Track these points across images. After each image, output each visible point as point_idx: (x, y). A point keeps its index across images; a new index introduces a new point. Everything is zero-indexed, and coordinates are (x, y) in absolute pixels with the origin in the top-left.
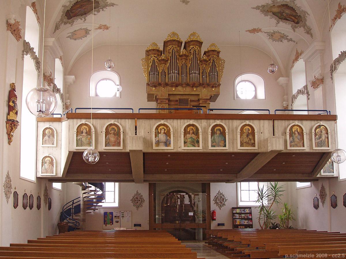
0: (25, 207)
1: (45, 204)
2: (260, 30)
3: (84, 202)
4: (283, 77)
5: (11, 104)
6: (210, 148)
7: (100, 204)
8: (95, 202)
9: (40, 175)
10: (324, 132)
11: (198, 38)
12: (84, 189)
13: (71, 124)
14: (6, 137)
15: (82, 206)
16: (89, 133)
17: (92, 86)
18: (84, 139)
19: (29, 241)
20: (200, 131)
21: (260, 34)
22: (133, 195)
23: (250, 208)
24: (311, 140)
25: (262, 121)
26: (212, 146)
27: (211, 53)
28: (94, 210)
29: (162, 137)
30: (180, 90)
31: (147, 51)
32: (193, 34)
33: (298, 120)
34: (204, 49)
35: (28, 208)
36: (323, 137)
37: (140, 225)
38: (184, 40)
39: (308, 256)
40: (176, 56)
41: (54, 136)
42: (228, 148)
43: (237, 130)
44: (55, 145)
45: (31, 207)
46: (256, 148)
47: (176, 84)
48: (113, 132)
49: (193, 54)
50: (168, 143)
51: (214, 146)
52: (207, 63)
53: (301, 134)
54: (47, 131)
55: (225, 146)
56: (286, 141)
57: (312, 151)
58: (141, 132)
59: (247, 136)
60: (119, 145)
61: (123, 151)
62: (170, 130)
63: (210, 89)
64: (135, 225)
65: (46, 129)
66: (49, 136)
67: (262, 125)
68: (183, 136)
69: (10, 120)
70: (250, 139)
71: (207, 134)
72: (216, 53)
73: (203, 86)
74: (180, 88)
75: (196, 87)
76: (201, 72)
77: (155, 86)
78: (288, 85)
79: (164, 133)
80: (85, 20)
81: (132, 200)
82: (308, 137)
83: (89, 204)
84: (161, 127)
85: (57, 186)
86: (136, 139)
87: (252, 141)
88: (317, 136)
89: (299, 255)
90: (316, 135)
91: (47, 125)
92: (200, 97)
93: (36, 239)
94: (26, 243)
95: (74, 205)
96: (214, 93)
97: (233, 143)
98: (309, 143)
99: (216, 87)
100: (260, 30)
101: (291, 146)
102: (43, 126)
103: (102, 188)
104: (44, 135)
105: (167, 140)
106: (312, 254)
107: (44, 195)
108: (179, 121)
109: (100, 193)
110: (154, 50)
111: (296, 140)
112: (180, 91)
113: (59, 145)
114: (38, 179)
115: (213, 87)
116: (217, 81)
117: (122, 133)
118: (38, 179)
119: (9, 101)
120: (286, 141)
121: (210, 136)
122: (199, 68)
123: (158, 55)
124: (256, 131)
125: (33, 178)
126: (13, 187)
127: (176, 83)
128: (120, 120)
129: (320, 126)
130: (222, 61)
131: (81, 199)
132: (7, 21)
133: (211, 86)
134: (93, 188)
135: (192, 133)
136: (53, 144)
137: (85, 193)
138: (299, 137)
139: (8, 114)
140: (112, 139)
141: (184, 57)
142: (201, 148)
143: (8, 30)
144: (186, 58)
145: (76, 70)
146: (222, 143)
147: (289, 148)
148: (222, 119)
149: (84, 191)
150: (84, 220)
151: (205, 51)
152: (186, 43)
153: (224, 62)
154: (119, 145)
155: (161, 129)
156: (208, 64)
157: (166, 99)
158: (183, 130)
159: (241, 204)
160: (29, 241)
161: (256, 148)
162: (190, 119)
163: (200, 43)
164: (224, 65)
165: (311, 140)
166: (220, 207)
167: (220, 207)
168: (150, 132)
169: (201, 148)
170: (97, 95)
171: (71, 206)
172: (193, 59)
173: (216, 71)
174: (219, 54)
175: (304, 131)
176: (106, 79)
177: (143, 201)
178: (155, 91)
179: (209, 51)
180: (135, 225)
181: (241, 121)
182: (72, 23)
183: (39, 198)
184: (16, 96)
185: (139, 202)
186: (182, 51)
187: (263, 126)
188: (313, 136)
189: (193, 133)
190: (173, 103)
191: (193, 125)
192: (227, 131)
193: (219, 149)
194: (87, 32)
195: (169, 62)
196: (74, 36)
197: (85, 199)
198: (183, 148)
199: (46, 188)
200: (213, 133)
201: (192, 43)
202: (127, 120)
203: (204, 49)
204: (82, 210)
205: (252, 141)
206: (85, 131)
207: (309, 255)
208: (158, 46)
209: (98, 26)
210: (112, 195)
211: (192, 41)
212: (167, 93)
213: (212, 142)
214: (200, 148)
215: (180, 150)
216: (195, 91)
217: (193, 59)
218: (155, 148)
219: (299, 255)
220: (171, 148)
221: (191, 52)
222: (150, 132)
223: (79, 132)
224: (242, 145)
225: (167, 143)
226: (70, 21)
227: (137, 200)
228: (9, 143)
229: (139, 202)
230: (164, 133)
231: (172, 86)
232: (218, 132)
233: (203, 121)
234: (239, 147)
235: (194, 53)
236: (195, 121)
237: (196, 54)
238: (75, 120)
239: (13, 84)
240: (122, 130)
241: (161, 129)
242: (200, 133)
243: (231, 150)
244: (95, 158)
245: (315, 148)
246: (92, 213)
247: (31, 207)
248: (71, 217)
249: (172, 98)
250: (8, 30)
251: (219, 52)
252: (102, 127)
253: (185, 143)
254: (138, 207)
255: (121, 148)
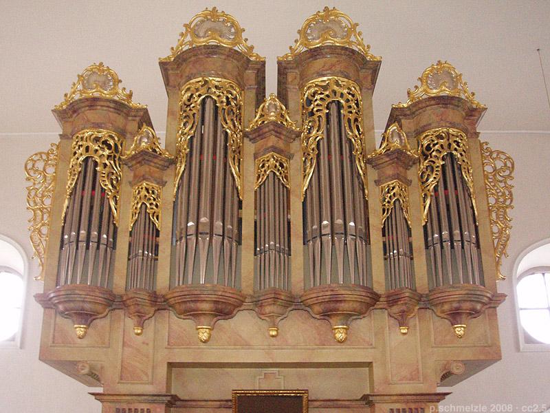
11: (353, 38)
32: (326, 19)
34: (391, 91)
39: (474, 408)
40: (221, 138)
47: (216, 302)
49: (324, 120)
52: (413, 174)
63: (434, 323)
73: (395, 309)
74: (244, 323)
75: (348, 317)
76: (376, 221)
77: (87, 317)
89: (457, 407)
99: (474, 313)
106: (482, 406)
116: (477, 282)
122: (366, 203)
127: (214, 297)
130: (499, 164)
133: (446, 307)
141: (272, 140)
144: (281, 145)
151: (393, 109)
153: (509, 164)
156: (415, 181)
157: (154, 398)
164: (509, 182)
172: (323, 145)
173: (471, 219)
174: (474, 124)
178: (85, 342)
179: (417, 107)
203: (391, 91)
207: (477, 407)
208: (121, 86)
212: (163, 357)
216: (340, 342)
217: (323, 145)
219: (457, 407)
221: (312, 114)
235: (334, 120)
237: (345, 124)
251: (473, 113)
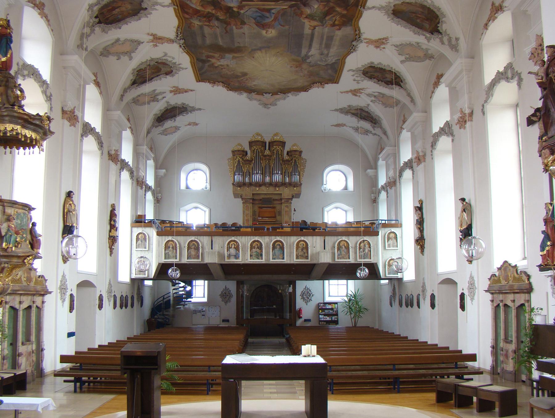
0: (121, 307)
1: (116, 212)
2: (345, 125)
3: (174, 298)
4: (372, 169)
5: (112, 223)
6: (272, 261)
7: (189, 300)
8: (185, 298)
9: (134, 276)
10: (367, 246)
12: (174, 286)
13: (160, 240)
14: (108, 250)
15: (172, 302)
16: (175, 248)
17: (183, 176)
18: (170, 253)
19: (128, 338)
20: (263, 246)
21: (345, 127)
22: (222, 290)
23: (336, 303)
24: (356, 253)
25: (315, 237)
26: (273, 259)
27: (293, 153)
28: (184, 305)
29: (233, 251)
30: (264, 190)
31: (233, 152)
33: (346, 236)
34: (287, 148)
35: (124, 307)
36: (367, 251)
37: (228, 321)
38: (267, 141)
41: (146, 241)
42: (286, 261)
43: (293, 245)
44: (147, 249)
45: (126, 307)
46: (309, 260)
48: (194, 247)
50: (237, 256)
51: (275, 259)
52: (290, 163)
53: (347, 248)
54: (140, 236)
55: (283, 259)
56: (334, 254)
57: (356, 262)
58: (216, 247)
59: (302, 250)
60: (198, 258)
61: (202, 263)
62: (239, 245)
63: (292, 188)
64: (224, 321)
65: (140, 233)
66: (141, 240)
67: (314, 240)
68: (249, 250)
69: (112, 236)
70: (305, 253)
71: (269, 248)
72: (298, 153)
74: (263, 188)
75: (278, 187)
76: (283, 171)
77: (240, 186)
78: (374, 180)
79: (235, 248)
80: (175, 120)
81: (220, 295)
82: (353, 250)
83: (179, 299)
84: (232, 243)
85: (149, 283)
86: (213, 252)
87: (306, 254)
88: (361, 250)
90: (360, 248)
91: (140, 230)
92: (283, 197)
93: (132, 336)
94: (126, 339)
95: (165, 300)
96: (296, 193)
97: (290, 256)
98: (354, 255)
100: (345, 125)
101: (338, 259)
102: (137, 231)
103: (190, 284)
104: (137, 239)
105: (237, 254)
107: (137, 294)
108: (246, 237)
109: (188, 288)
110: (239, 151)
111: (343, 253)
112: (263, 191)
113: (151, 249)
114: (132, 280)
115: (294, 187)
117: (200, 248)
118: (132, 280)
119: (111, 220)
120: (334, 254)
121: (271, 250)
123: (243, 155)
124: (309, 246)
125: (128, 280)
126: (113, 292)
128: (199, 237)
129: (364, 241)
131: (171, 294)
132: (109, 152)
134: (182, 284)
135: (257, 247)
136: (145, 248)
137: (174, 289)
138: (346, 250)
139: (110, 231)
140: (193, 252)
142: (264, 260)
143: (109, 159)
145: (167, 167)
146: (281, 257)
147: (336, 260)
148: (281, 235)
149: (174, 287)
150: (173, 316)
152: (269, 143)
154: (198, 258)
155: (232, 245)
158: (249, 246)
159: (328, 299)
160: (128, 338)
161: (309, 260)
162: (256, 236)
163: (283, 144)
165: (356, 253)
166: (306, 303)
167: (306, 303)
168: (223, 247)
169: (264, 260)
170: (187, 187)
171: (162, 302)
175: (350, 245)
176: (197, 170)
177: (231, 296)
179: (291, 151)
180: (224, 321)
181: (297, 237)
182: (162, 126)
183: (132, 297)
184: (116, 215)
185: (227, 297)
186: (267, 152)
187: (316, 242)
188: (358, 250)
189: (258, 248)
190: (257, 202)
191: (258, 241)
192: (285, 246)
193: (278, 261)
194: (177, 128)
195: (253, 162)
196: (165, 133)
197: (175, 295)
198: (249, 260)
199: (139, 286)
200: (274, 248)
201: (275, 143)
202: (205, 237)
203: (287, 148)
204: (171, 305)
205: (306, 254)
206: (171, 246)
209: (187, 123)
210: (200, 290)
211: (275, 141)
213: (273, 255)
214: (263, 261)
215: (247, 262)
218: (227, 261)
220: (240, 261)
222: (223, 247)
223: (167, 247)
224: (297, 258)
225: (237, 257)
226: (161, 124)
227: (225, 296)
228: (111, 255)
229: (227, 297)
230: (235, 248)
231: (256, 186)
232: (278, 247)
233: (266, 237)
234: (295, 260)
236: (260, 237)
238: (164, 237)
239: (114, 204)
240: (200, 246)
241: (232, 245)
242: (264, 248)
243: (289, 262)
244: (177, 274)
245: (358, 260)
246: (182, 309)
247: (126, 307)
248: (161, 313)
249: (256, 197)
250: (109, 159)
251: (301, 152)
252: (185, 244)
253: (251, 256)
254: (226, 303)
255: (200, 260)
